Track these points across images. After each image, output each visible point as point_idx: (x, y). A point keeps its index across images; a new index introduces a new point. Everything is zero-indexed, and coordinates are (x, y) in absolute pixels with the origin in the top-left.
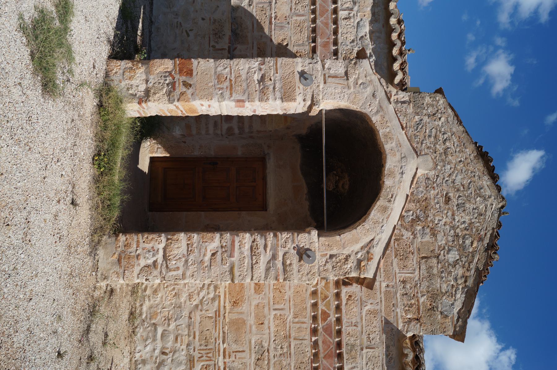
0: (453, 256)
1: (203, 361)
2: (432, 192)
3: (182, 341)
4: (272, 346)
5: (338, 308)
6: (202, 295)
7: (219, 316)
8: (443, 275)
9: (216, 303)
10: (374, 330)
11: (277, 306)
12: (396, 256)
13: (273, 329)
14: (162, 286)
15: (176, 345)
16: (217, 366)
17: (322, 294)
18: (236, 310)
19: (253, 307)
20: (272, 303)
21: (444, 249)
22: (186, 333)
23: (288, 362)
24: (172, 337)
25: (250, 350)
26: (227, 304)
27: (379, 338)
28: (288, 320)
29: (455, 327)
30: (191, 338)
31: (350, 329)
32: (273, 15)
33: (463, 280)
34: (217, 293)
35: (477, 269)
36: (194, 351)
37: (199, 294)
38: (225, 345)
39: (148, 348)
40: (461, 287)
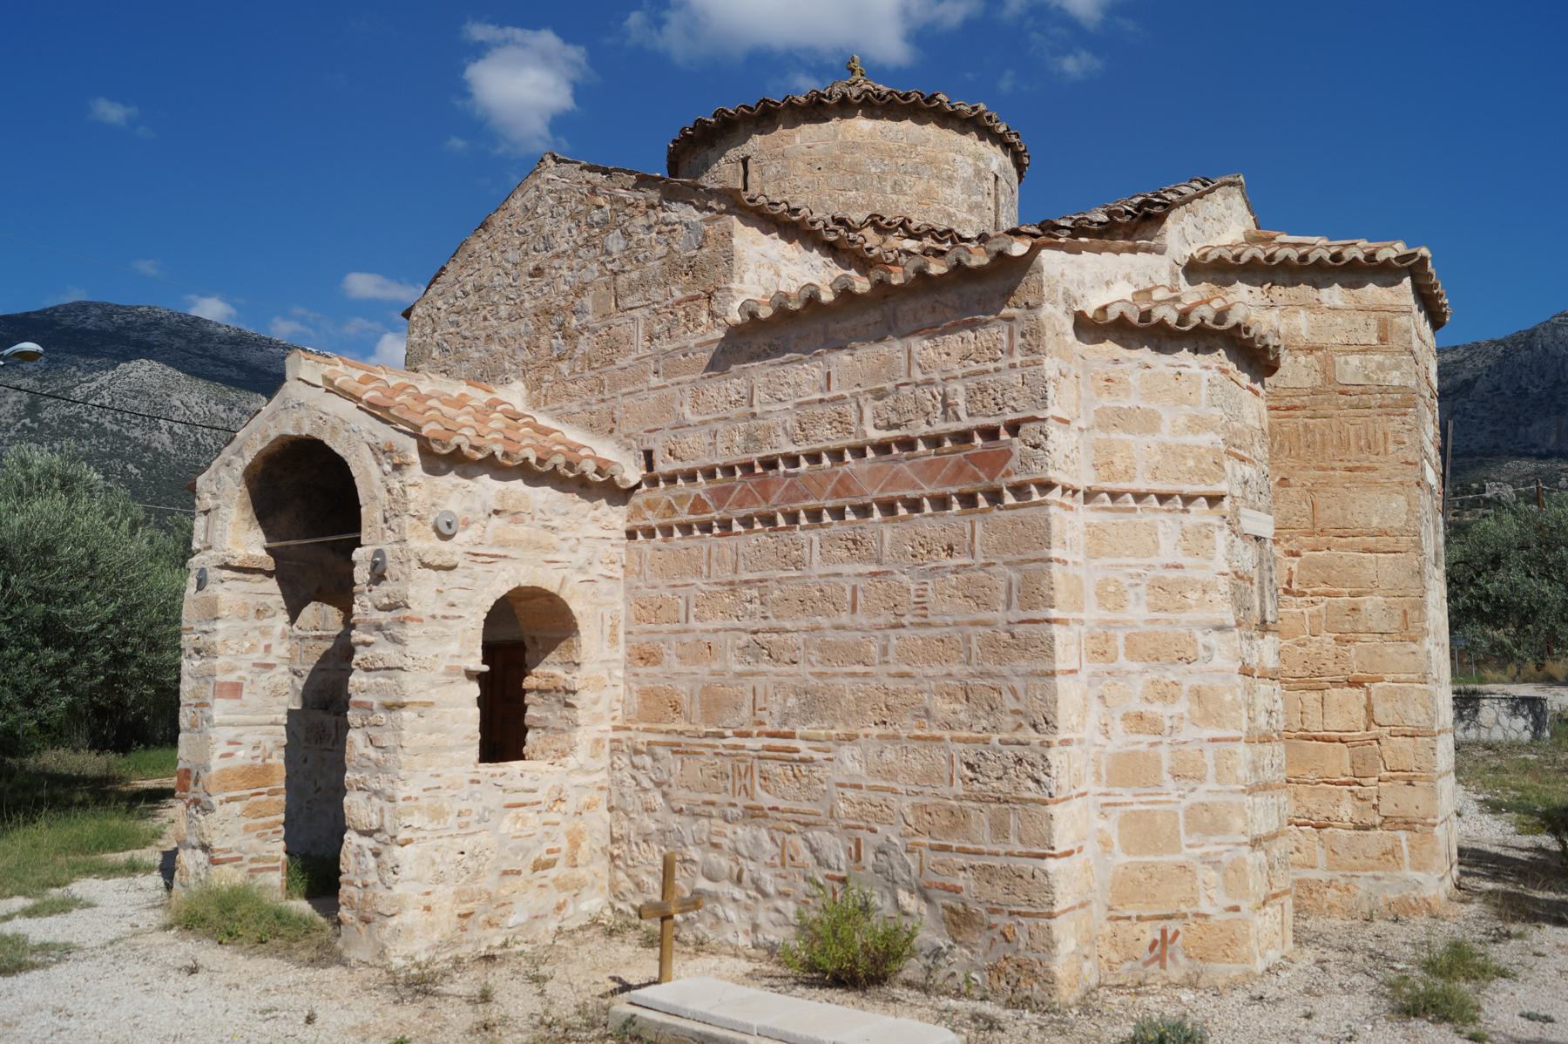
0: (615, 243)
1: (753, 788)
2: (527, 305)
3: (719, 834)
4: (746, 623)
5: (690, 476)
6: (646, 783)
7: (679, 745)
8: (641, 257)
9: (660, 751)
10: (723, 392)
11: (682, 616)
12: (612, 362)
13: (718, 623)
14: (631, 871)
15: (726, 848)
16: (762, 754)
17: (664, 516)
18: (686, 708)
19: (683, 669)
20: (676, 626)
21: (603, 263)
22: (705, 821)
23: (775, 585)
24: (713, 856)
25: (753, 674)
26: (663, 727)
27: (733, 384)
28: (704, 587)
29: (721, 212)
30: (714, 811)
31: (721, 447)
32: (314, 633)
33: (651, 212)
34: (644, 749)
35: (636, 187)
36: (734, 805)
37: (645, 790)
38: (729, 733)
39: (732, 915)
40: (662, 215)
